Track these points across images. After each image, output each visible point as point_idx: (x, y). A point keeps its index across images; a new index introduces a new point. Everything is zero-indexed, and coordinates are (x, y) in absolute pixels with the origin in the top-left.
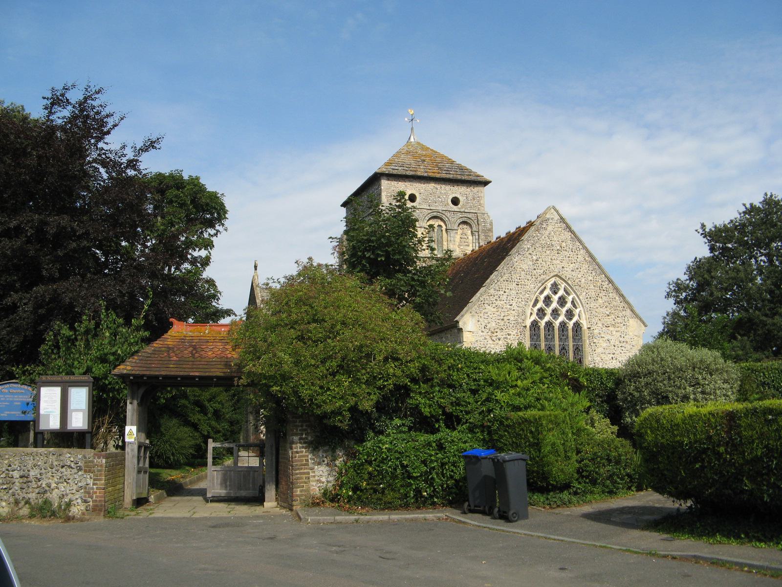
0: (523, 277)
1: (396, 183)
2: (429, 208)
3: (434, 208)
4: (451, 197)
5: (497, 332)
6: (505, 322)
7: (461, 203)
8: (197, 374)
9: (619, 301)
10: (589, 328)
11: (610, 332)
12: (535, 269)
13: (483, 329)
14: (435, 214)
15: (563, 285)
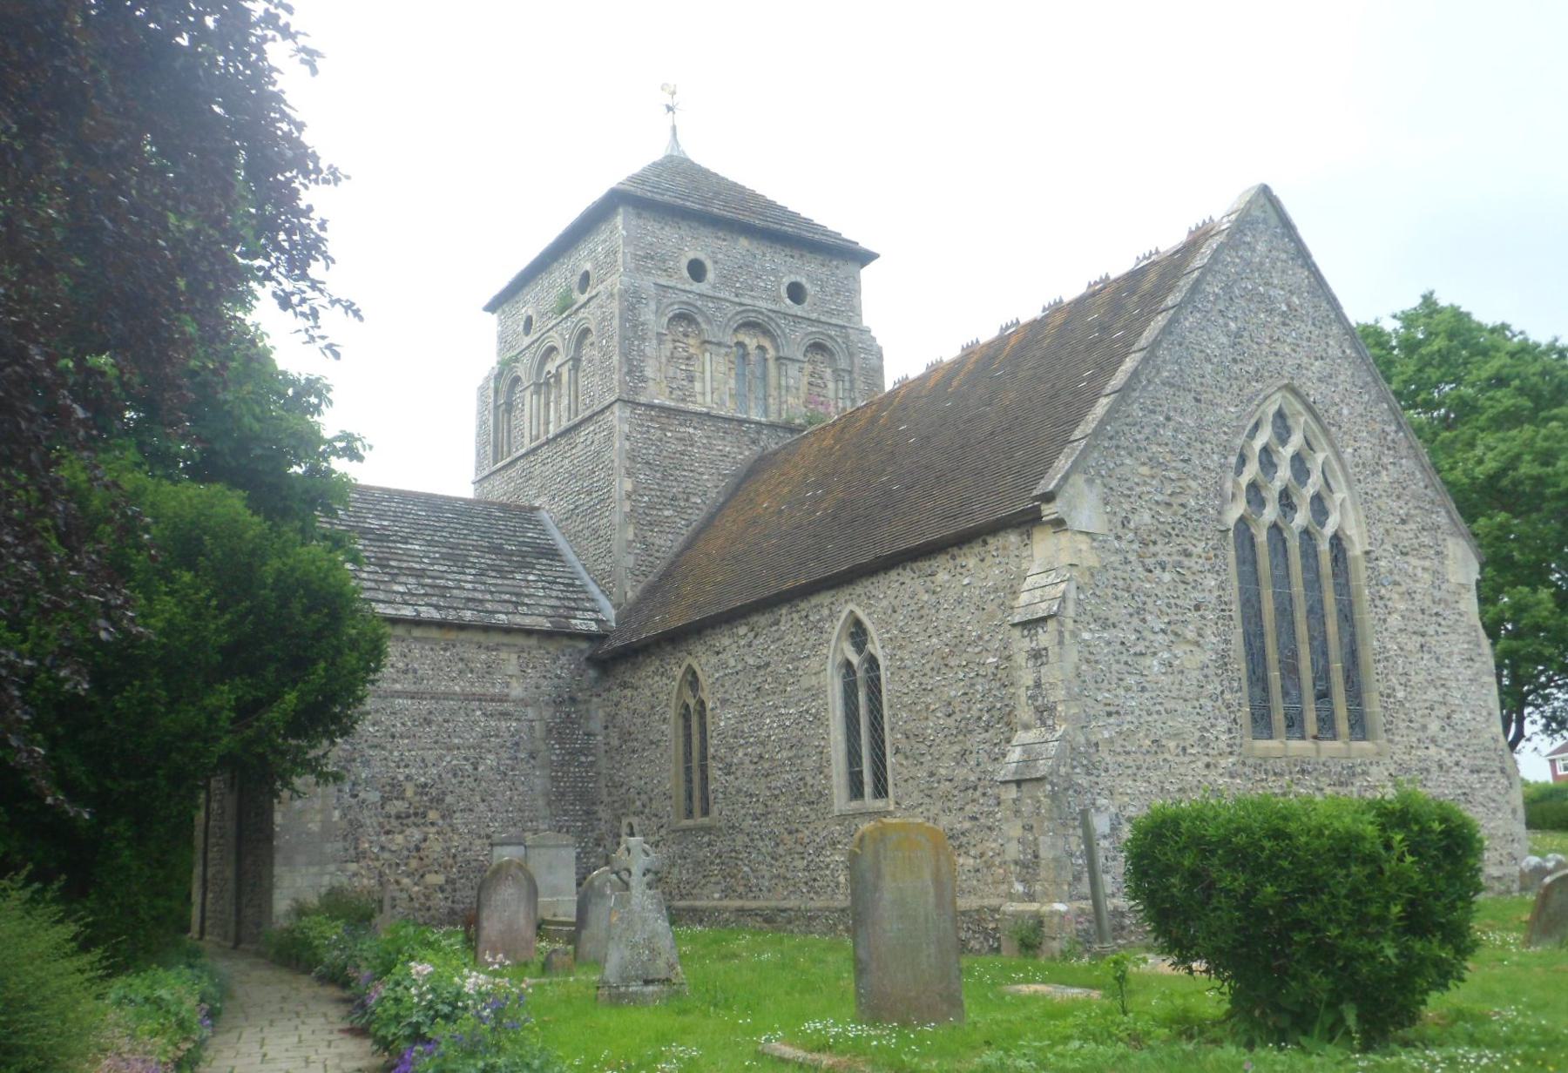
0: (1208, 380)
1: (657, 226)
3: (749, 301)
4: (786, 281)
5: (1155, 543)
6: (1175, 514)
10: (1367, 553)
12: (1235, 361)
14: (752, 317)
15: (1301, 423)
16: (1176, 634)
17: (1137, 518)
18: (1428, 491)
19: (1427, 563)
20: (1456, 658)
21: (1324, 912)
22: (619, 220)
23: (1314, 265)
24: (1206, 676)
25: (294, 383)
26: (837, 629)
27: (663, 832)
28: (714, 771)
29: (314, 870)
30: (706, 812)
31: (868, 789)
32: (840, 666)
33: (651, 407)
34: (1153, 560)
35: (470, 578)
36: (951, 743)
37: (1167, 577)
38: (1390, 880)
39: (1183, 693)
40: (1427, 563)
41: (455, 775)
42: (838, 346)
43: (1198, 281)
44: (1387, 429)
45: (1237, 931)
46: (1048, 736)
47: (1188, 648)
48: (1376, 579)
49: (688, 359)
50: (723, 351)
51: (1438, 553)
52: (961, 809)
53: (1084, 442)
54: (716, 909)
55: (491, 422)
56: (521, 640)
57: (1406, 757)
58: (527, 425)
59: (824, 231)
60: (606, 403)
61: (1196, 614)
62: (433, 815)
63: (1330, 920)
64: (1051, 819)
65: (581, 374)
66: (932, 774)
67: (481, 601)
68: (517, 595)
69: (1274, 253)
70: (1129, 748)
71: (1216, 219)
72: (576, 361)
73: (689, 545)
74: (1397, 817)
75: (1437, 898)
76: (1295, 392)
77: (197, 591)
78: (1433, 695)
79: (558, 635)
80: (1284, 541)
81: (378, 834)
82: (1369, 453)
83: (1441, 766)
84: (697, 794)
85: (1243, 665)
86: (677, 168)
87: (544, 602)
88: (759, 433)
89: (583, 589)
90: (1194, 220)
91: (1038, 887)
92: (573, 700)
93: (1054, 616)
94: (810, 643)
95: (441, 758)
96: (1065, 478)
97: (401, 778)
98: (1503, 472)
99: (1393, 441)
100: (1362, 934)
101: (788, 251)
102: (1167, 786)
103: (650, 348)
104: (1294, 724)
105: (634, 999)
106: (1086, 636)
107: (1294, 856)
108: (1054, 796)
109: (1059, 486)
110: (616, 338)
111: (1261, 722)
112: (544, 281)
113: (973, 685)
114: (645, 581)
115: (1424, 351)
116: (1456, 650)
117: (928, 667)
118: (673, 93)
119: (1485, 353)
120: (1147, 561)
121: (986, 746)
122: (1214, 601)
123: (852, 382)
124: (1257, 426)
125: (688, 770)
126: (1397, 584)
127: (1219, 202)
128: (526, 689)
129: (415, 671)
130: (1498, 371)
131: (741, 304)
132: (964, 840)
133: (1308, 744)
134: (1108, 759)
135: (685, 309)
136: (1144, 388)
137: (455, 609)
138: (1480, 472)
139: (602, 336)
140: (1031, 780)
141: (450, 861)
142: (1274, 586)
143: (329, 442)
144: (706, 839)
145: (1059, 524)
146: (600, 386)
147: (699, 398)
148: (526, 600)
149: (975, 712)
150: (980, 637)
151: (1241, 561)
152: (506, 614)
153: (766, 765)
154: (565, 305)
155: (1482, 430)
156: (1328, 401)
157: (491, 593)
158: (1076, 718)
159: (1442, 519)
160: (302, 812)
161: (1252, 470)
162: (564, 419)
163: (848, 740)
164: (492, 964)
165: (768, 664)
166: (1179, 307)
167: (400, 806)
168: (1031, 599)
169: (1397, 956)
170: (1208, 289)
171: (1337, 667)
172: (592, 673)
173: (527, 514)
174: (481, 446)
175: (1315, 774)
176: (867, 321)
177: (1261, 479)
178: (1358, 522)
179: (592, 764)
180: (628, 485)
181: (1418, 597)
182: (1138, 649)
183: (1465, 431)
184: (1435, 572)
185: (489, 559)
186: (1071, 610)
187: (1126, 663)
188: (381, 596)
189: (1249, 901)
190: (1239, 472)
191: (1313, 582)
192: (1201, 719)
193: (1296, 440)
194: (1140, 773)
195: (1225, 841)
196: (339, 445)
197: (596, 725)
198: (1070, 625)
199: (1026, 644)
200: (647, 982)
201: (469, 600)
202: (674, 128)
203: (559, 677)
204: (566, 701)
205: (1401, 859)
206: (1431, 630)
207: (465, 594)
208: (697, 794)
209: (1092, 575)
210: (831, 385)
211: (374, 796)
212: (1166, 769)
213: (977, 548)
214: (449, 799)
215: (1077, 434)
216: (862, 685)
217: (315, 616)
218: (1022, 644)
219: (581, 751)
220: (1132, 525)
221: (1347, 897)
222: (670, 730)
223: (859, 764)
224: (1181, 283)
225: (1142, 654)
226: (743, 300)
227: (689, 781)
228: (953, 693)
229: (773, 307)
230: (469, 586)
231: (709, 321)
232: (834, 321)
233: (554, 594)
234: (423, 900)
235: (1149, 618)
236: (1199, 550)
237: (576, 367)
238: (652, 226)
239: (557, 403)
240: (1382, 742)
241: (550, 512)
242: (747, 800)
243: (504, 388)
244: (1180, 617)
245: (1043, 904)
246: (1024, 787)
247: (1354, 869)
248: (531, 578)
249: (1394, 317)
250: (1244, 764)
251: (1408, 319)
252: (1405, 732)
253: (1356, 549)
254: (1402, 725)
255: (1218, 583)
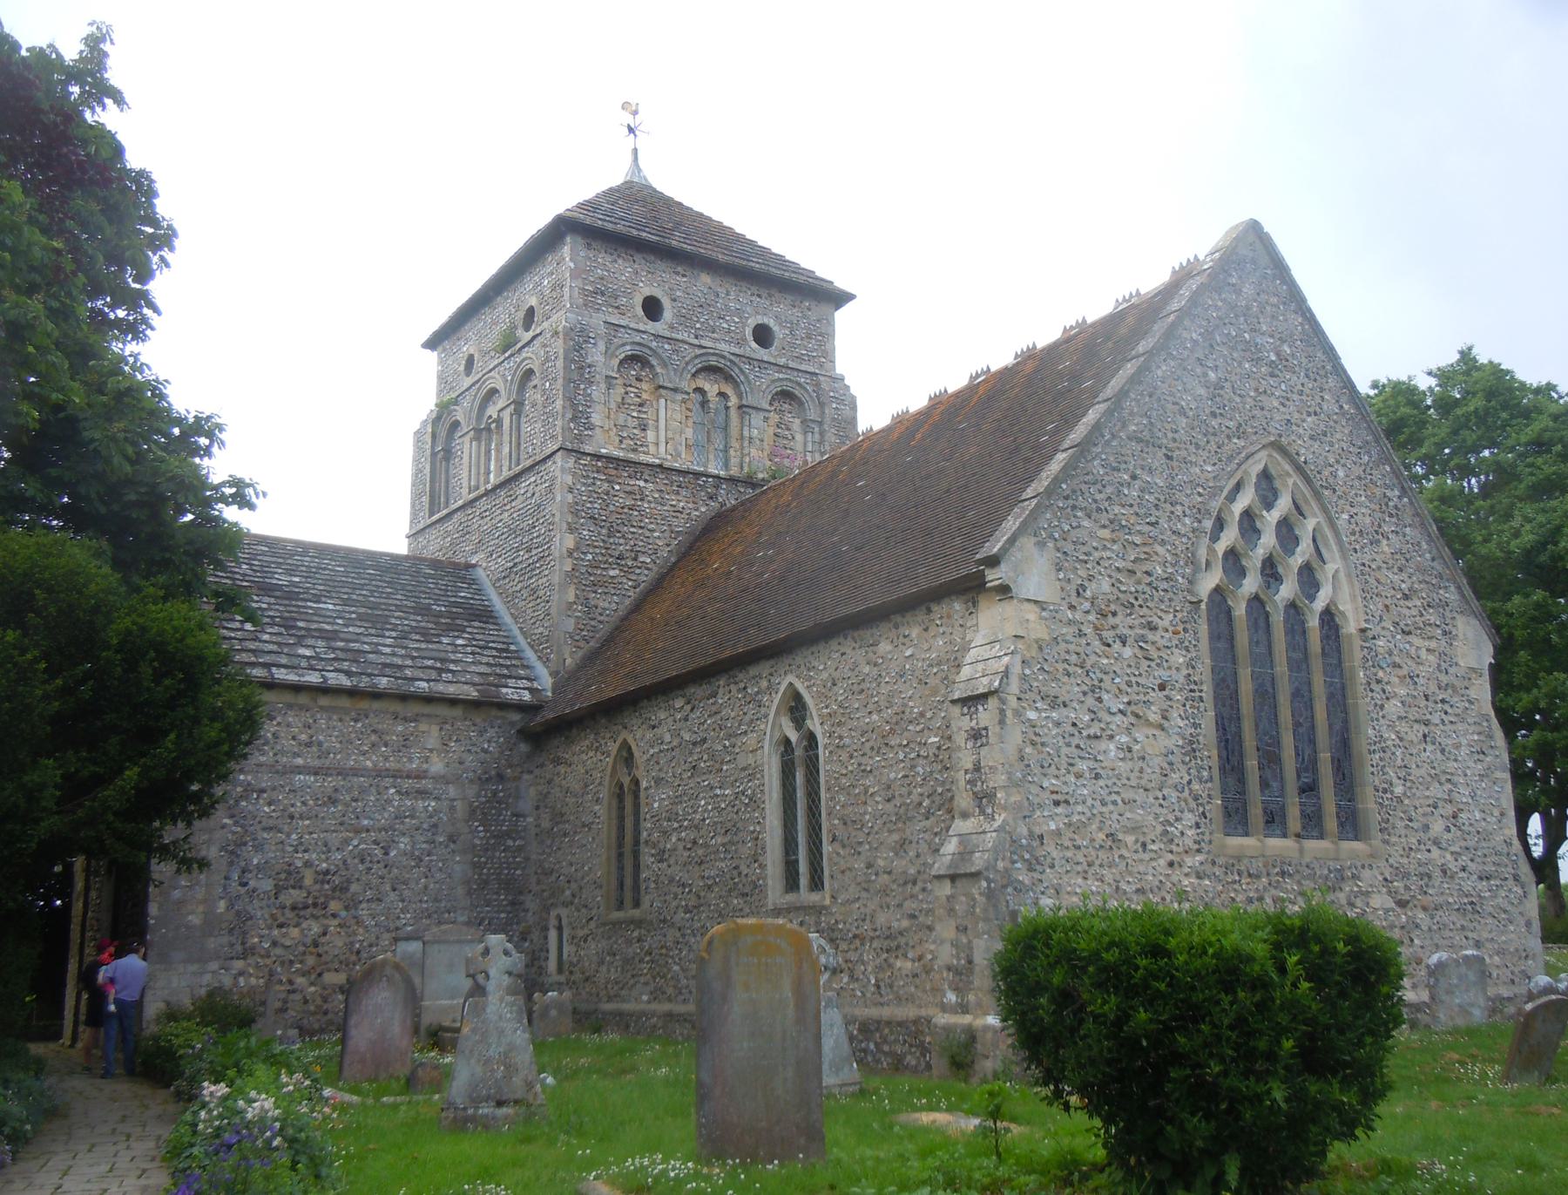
2: (696, 342)
4: (752, 322)
8: (78, 906)
9: (1428, 556)
10: (1363, 631)
11: (1413, 651)
12: (1214, 415)
13: (1074, 600)
14: (713, 361)
15: (1289, 483)
16: (1137, 716)
17: (1094, 585)
18: (1435, 564)
19: (1433, 644)
20: (1464, 751)
21: (1206, 1045)
22: (566, 250)
23: (1309, 310)
24: (1171, 764)
25: (179, 421)
26: (776, 701)
27: (592, 924)
28: (647, 858)
29: (194, 968)
30: (637, 904)
31: (804, 881)
32: (778, 743)
33: (598, 457)
34: (1112, 633)
35: (388, 641)
36: (890, 831)
37: (1128, 652)
38: (1282, 1008)
39: (1143, 782)
40: (1433, 644)
41: (362, 861)
42: (809, 392)
43: (1173, 325)
44: (1389, 493)
45: (1109, 1063)
46: (986, 826)
47: (1151, 731)
48: (1372, 660)
49: (641, 405)
50: (679, 397)
51: (1445, 633)
52: (900, 906)
53: (1035, 501)
54: (643, 1013)
55: (427, 470)
57: (1405, 861)
58: (465, 474)
59: (796, 268)
60: (549, 452)
61: (1161, 694)
62: (334, 906)
63: (1211, 1055)
64: (986, 920)
65: (523, 420)
66: (869, 866)
67: (400, 667)
68: (442, 660)
69: (1264, 297)
70: (1079, 842)
71: (1201, 258)
72: (518, 405)
73: (637, 607)
74: (1295, 936)
75: (1341, 1032)
76: (1283, 450)
77: (23, 651)
78: (1436, 791)
79: (486, 705)
80: (1267, 615)
81: (270, 928)
82: (1368, 520)
83: (1444, 872)
84: (628, 882)
85: (1215, 752)
86: (636, 196)
87: (473, 668)
88: (717, 487)
89: (518, 656)
90: (1179, 258)
91: (971, 997)
92: (501, 777)
93: (996, 692)
94: (747, 718)
95: (347, 841)
96: (1012, 540)
97: (299, 864)
98: (1541, 546)
99: (1396, 507)
100: (1246, 1075)
101: (754, 289)
102: (1123, 886)
103: (597, 392)
104: (1274, 820)
105: (486, 1124)
106: (1032, 715)
107: (1172, 977)
108: (990, 895)
109: (1004, 550)
110: (560, 381)
111: (1236, 817)
112: (487, 316)
113: (913, 767)
114: (586, 647)
115: (1459, 412)
116: (1464, 742)
117: (868, 745)
118: (635, 113)
119: (1527, 414)
120: (1104, 634)
121: (926, 836)
122: (1182, 680)
123: (822, 434)
124: (1238, 487)
125: (620, 855)
126: (1397, 666)
127: (1199, 238)
128: (447, 765)
129: (320, 744)
130: (1540, 435)
131: (701, 347)
132: (902, 941)
133: (1289, 843)
134: (1055, 854)
135: (638, 351)
136: (1108, 443)
137: (369, 675)
138: (1515, 545)
139: (545, 378)
140: (966, 875)
141: (354, 958)
142: (1253, 665)
143: (216, 488)
144: (636, 934)
145: (1004, 590)
146: (541, 434)
147: (652, 449)
148: (452, 667)
149: (915, 798)
150: (922, 714)
151: (1214, 637)
152: (428, 681)
153: (700, 852)
154: (508, 344)
155: (1521, 500)
156: (1320, 461)
157: (413, 658)
158: (1018, 807)
159: (1452, 595)
160: (181, 903)
161: (1230, 536)
162: (505, 469)
163: (785, 826)
164: (287, 1085)
165: (704, 740)
166: (1149, 353)
167: (295, 895)
168: (974, 673)
169: (1287, 1100)
170: (1185, 334)
171: (1325, 757)
172: (524, 747)
173: (461, 572)
174: (416, 497)
175: (1297, 877)
176: (841, 368)
177: (1241, 546)
178: (1353, 597)
179: (520, 849)
180: (570, 541)
181: (1421, 681)
182: (1092, 731)
183: (1503, 499)
184: (1442, 654)
185: (414, 621)
186: (1014, 687)
187: (1078, 747)
188: (284, 661)
189: (1121, 1029)
190: (1215, 538)
191: (1300, 663)
192: (1164, 811)
193: (1283, 504)
194: (1092, 871)
195: (1095, 956)
196: (228, 491)
197: (526, 805)
198: (1013, 702)
199: (966, 723)
200: (500, 1104)
201: (385, 665)
202: (635, 151)
203: (485, 751)
204: (494, 779)
205: (1295, 985)
206: (1435, 719)
207: (382, 659)
208: (628, 882)
209: (1040, 648)
210: (799, 437)
211: (267, 885)
212: (1122, 866)
213: (921, 616)
214: (354, 888)
215: (1029, 492)
216: (800, 761)
217: (167, 682)
218: (962, 723)
219: (508, 834)
220: (1088, 593)
221: (1231, 1027)
222: (601, 811)
223: (796, 853)
224: (1156, 327)
225: (1096, 737)
226: (703, 342)
227: (621, 868)
228: (892, 775)
229: (737, 351)
230: (388, 650)
231: (664, 365)
232: (803, 367)
233: (485, 660)
234: (319, 1001)
235: (1105, 697)
236: (1166, 623)
237: (518, 412)
238: (603, 258)
239: (498, 451)
240: (1376, 842)
241: (486, 568)
242: (680, 890)
243: (443, 434)
244: (1141, 697)
245: (976, 1017)
246: (959, 883)
247: (1241, 995)
248: (460, 642)
249: (1430, 374)
250: (1214, 863)
251: (1444, 376)
252: (1403, 832)
253: (1350, 626)
254: (1400, 824)
255: (1186, 660)
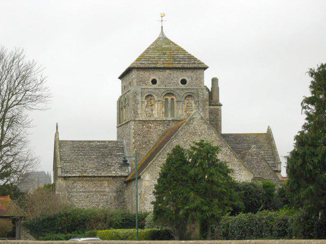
4: (180, 79)
7: (188, 83)
14: (169, 92)
33: (140, 121)
50: (160, 102)
56: (108, 179)
202: (162, 27)
